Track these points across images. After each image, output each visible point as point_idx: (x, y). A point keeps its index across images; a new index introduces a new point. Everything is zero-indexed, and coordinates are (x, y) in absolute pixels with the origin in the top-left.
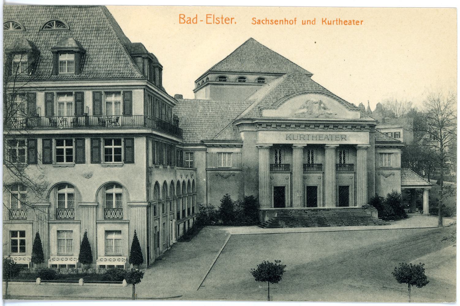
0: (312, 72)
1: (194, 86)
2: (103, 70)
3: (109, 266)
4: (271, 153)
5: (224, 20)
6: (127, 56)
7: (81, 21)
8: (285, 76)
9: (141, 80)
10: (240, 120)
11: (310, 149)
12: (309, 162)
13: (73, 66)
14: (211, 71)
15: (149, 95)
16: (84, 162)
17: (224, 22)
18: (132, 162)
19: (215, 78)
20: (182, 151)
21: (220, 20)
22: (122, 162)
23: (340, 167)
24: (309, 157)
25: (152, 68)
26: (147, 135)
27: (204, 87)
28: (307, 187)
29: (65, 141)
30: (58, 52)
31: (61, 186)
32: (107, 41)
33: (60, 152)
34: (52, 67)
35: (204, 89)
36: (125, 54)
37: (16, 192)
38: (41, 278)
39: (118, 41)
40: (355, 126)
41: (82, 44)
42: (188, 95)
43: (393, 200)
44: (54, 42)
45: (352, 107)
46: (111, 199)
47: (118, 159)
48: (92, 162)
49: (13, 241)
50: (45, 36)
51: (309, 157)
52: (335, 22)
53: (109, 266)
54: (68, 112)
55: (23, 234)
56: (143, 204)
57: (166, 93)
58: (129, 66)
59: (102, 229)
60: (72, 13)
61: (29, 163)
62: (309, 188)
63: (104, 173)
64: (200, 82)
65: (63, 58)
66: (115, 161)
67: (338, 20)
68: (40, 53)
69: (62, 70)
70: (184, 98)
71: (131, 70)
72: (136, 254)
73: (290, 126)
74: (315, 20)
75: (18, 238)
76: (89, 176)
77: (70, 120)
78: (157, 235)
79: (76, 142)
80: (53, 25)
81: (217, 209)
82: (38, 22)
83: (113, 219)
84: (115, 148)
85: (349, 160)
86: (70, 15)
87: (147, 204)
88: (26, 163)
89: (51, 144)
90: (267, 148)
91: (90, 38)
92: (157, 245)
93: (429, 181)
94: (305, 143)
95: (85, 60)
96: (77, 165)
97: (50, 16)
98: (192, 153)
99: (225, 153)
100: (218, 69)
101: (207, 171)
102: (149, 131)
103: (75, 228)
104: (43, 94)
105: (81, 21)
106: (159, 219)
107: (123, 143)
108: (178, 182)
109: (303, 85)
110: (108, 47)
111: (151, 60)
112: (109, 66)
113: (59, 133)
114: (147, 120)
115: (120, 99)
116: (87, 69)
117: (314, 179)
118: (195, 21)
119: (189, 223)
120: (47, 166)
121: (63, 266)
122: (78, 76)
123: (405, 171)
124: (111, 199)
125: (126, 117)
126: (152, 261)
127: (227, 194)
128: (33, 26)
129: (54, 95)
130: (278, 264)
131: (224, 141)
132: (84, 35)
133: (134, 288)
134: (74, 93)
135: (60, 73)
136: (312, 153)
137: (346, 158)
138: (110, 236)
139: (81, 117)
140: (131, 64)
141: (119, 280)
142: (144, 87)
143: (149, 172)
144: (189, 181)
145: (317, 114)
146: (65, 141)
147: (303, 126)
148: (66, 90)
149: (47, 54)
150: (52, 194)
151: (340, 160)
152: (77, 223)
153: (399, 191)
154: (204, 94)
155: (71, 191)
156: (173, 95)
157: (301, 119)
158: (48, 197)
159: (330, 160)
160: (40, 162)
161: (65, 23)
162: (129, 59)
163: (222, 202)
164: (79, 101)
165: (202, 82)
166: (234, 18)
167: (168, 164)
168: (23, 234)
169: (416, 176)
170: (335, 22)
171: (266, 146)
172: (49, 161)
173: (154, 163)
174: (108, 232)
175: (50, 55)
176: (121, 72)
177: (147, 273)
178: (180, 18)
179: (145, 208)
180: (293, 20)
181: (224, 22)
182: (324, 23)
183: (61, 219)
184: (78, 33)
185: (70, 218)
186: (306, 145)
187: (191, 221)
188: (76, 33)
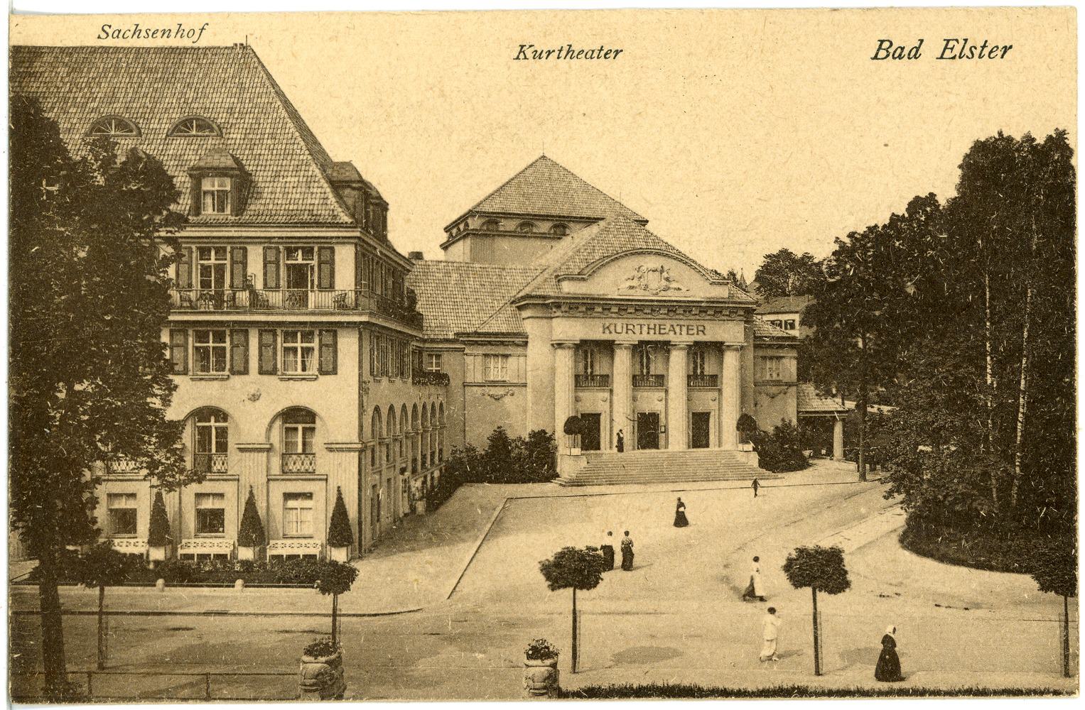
0: (646, 218)
1: (444, 237)
2: (283, 208)
4: (576, 354)
6: (326, 185)
7: (242, 121)
8: (602, 223)
9: (350, 227)
10: (523, 298)
11: (641, 350)
12: (586, 372)
14: (471, 213)
15: (364, 255)
16: (245, 372)
18: (334, 371)
19: (480, 226)
20: (420, 353)
23: (638, 381)
24: (641, 363)
25: (369, 209)
27: (459, 240)
28: (693, 413)
29: (299, 335)
30: (197, 175)
32: (289, 158)
34: (189, 202)
35: (461, 243)
36: (322, 181)
39: (310, 157)
40: (714, 309)
41: (244, 162)
42: (433, 253)
44: (193, 158)
47: (220, 366)
48: (262, 372)
50: (178, 144)
51: (641, 363)
53: (217, 555)
56: (355, 446)
57: (394, 250)
58: (329, 202)
59: (278, 490)
60: (227, 106)
64: (454, 231)
70: (427, 257)
71: (333, 210)
72: (340, 530)
73: (721, 312)
76: (255, 398)
78: (376, 504)
79: (231, 336)
80: (192, 127)
82: (165, 121)
83: (299, 472)
85: (600, 369)
86: (222, 110)
87: (360, 446)
91: (259, 152)
92: (376, 518)
93: (843, 404)
94: (635, 338)
95: (249, 190)
97: (187, 111)
98: (438, 357)
100: (487, 208)
101: (464, 386)
102: (364, 319)
103: (228, 488)
104: (260, 249)
105: (242, 121)
106: (380, 471)
107: (228, 339)
109: (631, 240)
110: (291, 169)
111: (365, 189)
112: (292, 202)
113: (244, 320)
114: (360, 298)
116: (254, 207)
117: (651, 401)
119: (432, 478)
120: (266, 378)
121: (203, 557)
122: (237, 218)
123: (804, 387)
125: (323, 293)
127: (499, 428)
128: (155, 127)
129: (280, 252)
131: (496, 335)
132: (248, 146)
135: (203, 213)
136: (592, 355)
137: (706, 366)
138: (291, 503)
139: (241, 293)
140: (334, 200)
142: (356, 241)
143: (363, 389)
145: (653, 288)
146: (299, 335)
147: (584, 309)
148: (205, 243)
151: (586, 368)
152: (320, 480)
154: (461, 250)
157: (646, 298)
159: (677, 366)
162: (328, 190)
163: (491, 440)
164: (326, 263)
165: (457, 231)
171: (569, 344)
172: (242, 369)
173: (372, 373)
174: (288, 496)
176: (315, 212)
177: (364, 568)
179: (357, 454)
183: (291, 472)
184: (238, 142)
185: (307, 472)
186: (637, 343)
187: (437, 474)
188: (233, 141)
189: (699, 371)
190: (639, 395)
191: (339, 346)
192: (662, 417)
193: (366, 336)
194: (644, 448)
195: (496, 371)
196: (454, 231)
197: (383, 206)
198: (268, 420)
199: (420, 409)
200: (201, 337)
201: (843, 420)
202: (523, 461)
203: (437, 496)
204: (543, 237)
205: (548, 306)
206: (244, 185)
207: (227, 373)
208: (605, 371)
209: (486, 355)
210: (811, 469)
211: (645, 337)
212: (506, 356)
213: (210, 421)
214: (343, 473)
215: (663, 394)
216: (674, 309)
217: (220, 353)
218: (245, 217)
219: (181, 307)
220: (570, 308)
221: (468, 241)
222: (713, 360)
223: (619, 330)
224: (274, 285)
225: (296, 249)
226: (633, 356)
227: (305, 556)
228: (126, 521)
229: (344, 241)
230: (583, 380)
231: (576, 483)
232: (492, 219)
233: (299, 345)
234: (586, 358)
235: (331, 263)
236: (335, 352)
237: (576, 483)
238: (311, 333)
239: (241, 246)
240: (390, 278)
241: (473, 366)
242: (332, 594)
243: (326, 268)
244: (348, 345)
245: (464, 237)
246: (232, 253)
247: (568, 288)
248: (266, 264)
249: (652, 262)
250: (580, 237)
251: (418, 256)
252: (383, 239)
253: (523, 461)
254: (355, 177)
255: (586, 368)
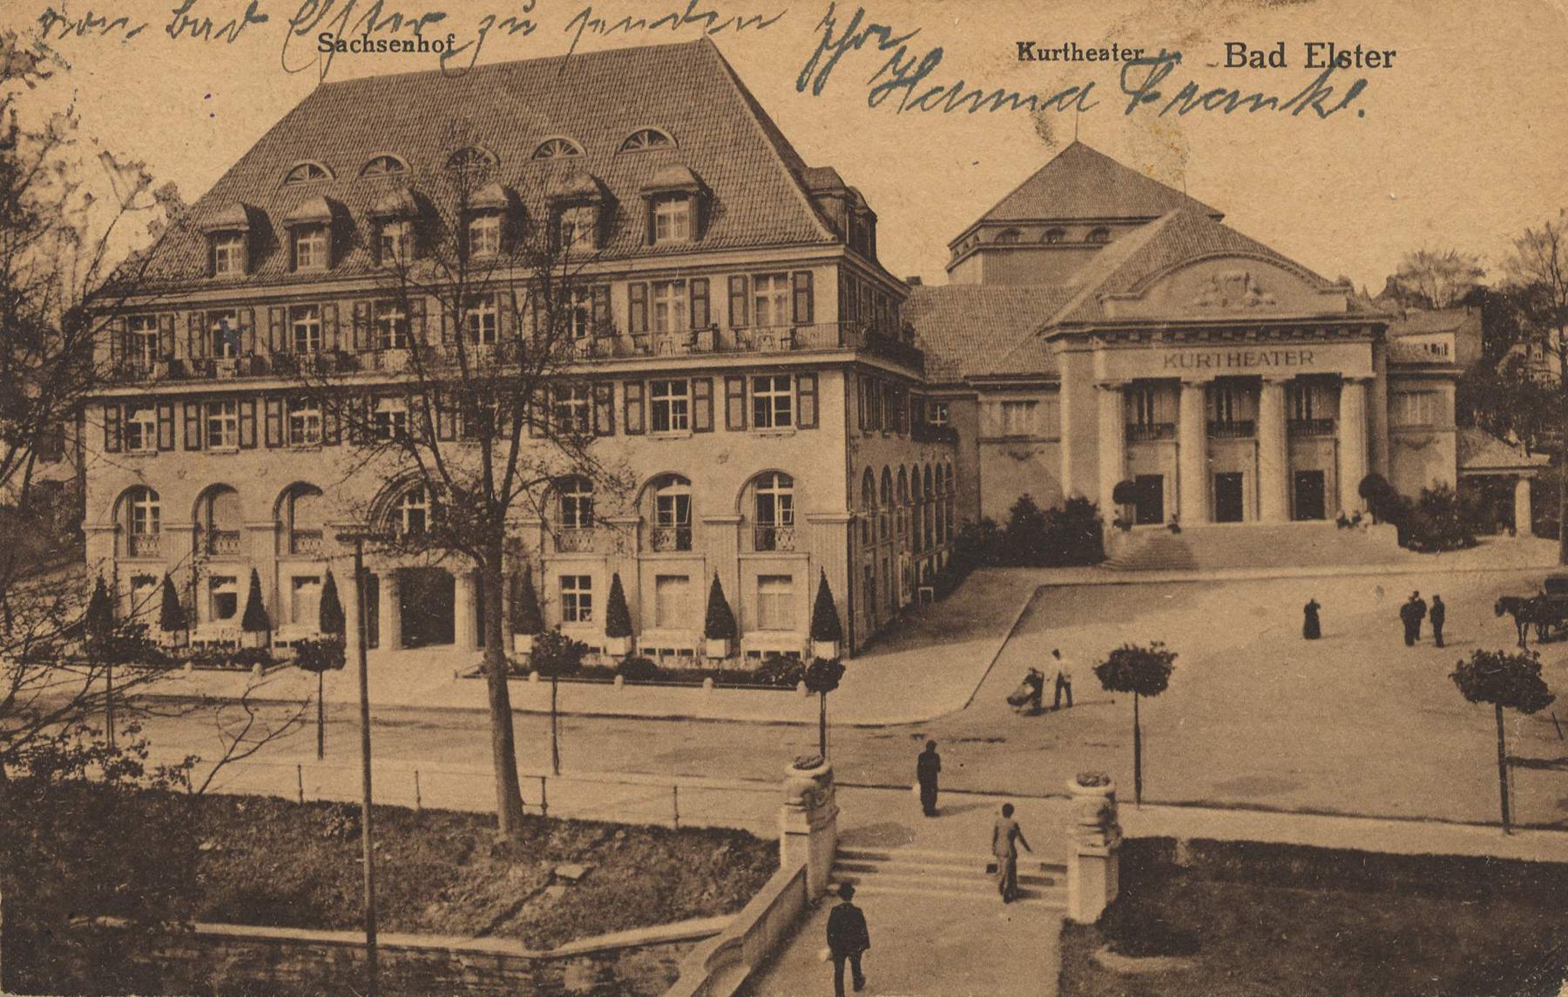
1: (947, 255)
3: (768, 654)
4: (1127, 400)
5: (1363, 57)
11: (1298, 388)
13: (686, 225)
14: (983, 223)
15: (848, 278)
17: (1363, 62)
19: (995, 237)
21: (1353, 58)
22: (793, 426)
24: (1220, 408)
25: (856, 225)
26: (844, 368)
30: (559, 204)
31: (664, 480)
33: (761, 405)
37: (141, 504)
38: (541, 674)
40: (1328, 329)
42: (934, 276)
43: (1434, 501)
45: (1326, 290)
46: (769, 509)
47: (784, 420)
49: (565, 596)
52: (1061, 56)
54: (779, 316)
55: (586, 582)
61: (598, 433)
62: (1221, 478)
63: (759, 450)
65: (570, 216)
66: (777, 424)
67: (1070, 47)
68: (618, 201)
69: (663, 234)
72: (824, 623)
74: (1282, 54)
75: (577, 591)
77: (780, 333)
78: (870, 585)
81: (1003, 527)
84: (773, 396)
88: (591, 434)
89: (744, 388)
90: (1118, 389)
96: (799, 433)
99: (1019, 404)
100: (997, 216)
102: (850, 357)
108: (939, 466)
111: (851, 198)
115: (786, 290)
116: (717, 228)
118: (1277, 59)
124: (769, 509)
126: (859, 643)
130: (1157, 650)
133: (823, 700)
134: (790, 275)
138: (768, 589)
141: (788, 683)
143: (852, 447)
144: (939, 466)
149: (631, 203)
150: (646, 498)
151: (1299, 411)
153: (1452, 482)
155: (683, 490)
156: (902, 278)
158: (637, 503)
160: (620, 430)
161: (666, 134)
165: (963, 247)
166: (1394, 53)
167: (891, 430)
168: (586, 582)
169: (1495, 444)
170: (1061, 56)
171: (1115, 384)
173: (861, 426)
175: (642, 206)
178: (1230, 53)
179: (190, 535)
180: (1353, 49)
181: (1363, 62)
182: (1025, 55)
187: (945, 555)
189: (1146, 420)
190: (1136, 450)
191: (821, 391)
192: (1328, 476)
193: (852, 377)
194: (1299, 519)
195: (1023, 421)
196: (960, 249)
197: (872, 218)
198: (738, 488)
199: (894, 475)
200: (660, 389)
201: (1530, 480)
202: (1064, 536)
203: (947, 581)
204: (1076, 247)
205: (1077, 334)
206: (706, 206)
207: (793, 426)
208: (1247, 416)
209: (1005, 404)
210: (1475, 550)
211: (1225, 371)
212: (1031, 404)
213: (771, 487)
214: (832, 550)
215: (1253, 447)
216: (1267, 332)
217: (783, 403)
218: (707, 240)
219: (634, 354)
220: (1118, 337)
221: (980, 259)
222: (1246, 401)
223: (1186, 361)
224: (806, 319)
225: (666, 284)
226: (1288, 398)
227: (788, 653)
228: (577, 608)
229: (827, 261)
230: (1133, 434)
231: (1133, 566)
232: (1010, 230)
233: (670, 398)
234: (1219, 400)
235: (809, 291)
236: (816, 402)
237: (1133, 566)
238: (788, 380)
239: (700, 276)
240: (877, 305)
241: (992, 417)
242: (818, 693)
243: (803, 297)
244: (833, 391)
245: (974, 254)
246: (794, 279)
247: (1111, 311)
248: (632, 302)
249: (1230, 270)
250: (1124, 246)
251: (916, 281)
252: (873, 259)
253: (1064, 536)
254: (835, 182)
255: (1141, 416)
